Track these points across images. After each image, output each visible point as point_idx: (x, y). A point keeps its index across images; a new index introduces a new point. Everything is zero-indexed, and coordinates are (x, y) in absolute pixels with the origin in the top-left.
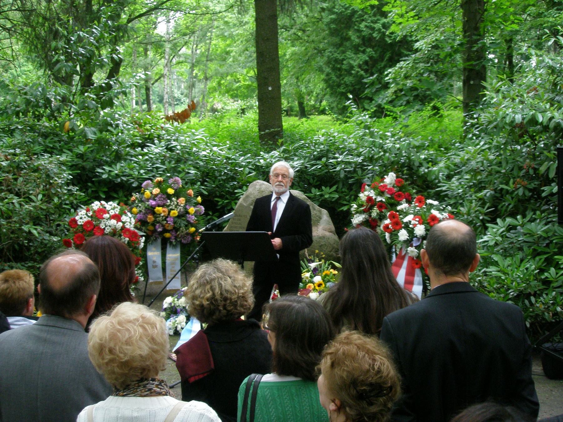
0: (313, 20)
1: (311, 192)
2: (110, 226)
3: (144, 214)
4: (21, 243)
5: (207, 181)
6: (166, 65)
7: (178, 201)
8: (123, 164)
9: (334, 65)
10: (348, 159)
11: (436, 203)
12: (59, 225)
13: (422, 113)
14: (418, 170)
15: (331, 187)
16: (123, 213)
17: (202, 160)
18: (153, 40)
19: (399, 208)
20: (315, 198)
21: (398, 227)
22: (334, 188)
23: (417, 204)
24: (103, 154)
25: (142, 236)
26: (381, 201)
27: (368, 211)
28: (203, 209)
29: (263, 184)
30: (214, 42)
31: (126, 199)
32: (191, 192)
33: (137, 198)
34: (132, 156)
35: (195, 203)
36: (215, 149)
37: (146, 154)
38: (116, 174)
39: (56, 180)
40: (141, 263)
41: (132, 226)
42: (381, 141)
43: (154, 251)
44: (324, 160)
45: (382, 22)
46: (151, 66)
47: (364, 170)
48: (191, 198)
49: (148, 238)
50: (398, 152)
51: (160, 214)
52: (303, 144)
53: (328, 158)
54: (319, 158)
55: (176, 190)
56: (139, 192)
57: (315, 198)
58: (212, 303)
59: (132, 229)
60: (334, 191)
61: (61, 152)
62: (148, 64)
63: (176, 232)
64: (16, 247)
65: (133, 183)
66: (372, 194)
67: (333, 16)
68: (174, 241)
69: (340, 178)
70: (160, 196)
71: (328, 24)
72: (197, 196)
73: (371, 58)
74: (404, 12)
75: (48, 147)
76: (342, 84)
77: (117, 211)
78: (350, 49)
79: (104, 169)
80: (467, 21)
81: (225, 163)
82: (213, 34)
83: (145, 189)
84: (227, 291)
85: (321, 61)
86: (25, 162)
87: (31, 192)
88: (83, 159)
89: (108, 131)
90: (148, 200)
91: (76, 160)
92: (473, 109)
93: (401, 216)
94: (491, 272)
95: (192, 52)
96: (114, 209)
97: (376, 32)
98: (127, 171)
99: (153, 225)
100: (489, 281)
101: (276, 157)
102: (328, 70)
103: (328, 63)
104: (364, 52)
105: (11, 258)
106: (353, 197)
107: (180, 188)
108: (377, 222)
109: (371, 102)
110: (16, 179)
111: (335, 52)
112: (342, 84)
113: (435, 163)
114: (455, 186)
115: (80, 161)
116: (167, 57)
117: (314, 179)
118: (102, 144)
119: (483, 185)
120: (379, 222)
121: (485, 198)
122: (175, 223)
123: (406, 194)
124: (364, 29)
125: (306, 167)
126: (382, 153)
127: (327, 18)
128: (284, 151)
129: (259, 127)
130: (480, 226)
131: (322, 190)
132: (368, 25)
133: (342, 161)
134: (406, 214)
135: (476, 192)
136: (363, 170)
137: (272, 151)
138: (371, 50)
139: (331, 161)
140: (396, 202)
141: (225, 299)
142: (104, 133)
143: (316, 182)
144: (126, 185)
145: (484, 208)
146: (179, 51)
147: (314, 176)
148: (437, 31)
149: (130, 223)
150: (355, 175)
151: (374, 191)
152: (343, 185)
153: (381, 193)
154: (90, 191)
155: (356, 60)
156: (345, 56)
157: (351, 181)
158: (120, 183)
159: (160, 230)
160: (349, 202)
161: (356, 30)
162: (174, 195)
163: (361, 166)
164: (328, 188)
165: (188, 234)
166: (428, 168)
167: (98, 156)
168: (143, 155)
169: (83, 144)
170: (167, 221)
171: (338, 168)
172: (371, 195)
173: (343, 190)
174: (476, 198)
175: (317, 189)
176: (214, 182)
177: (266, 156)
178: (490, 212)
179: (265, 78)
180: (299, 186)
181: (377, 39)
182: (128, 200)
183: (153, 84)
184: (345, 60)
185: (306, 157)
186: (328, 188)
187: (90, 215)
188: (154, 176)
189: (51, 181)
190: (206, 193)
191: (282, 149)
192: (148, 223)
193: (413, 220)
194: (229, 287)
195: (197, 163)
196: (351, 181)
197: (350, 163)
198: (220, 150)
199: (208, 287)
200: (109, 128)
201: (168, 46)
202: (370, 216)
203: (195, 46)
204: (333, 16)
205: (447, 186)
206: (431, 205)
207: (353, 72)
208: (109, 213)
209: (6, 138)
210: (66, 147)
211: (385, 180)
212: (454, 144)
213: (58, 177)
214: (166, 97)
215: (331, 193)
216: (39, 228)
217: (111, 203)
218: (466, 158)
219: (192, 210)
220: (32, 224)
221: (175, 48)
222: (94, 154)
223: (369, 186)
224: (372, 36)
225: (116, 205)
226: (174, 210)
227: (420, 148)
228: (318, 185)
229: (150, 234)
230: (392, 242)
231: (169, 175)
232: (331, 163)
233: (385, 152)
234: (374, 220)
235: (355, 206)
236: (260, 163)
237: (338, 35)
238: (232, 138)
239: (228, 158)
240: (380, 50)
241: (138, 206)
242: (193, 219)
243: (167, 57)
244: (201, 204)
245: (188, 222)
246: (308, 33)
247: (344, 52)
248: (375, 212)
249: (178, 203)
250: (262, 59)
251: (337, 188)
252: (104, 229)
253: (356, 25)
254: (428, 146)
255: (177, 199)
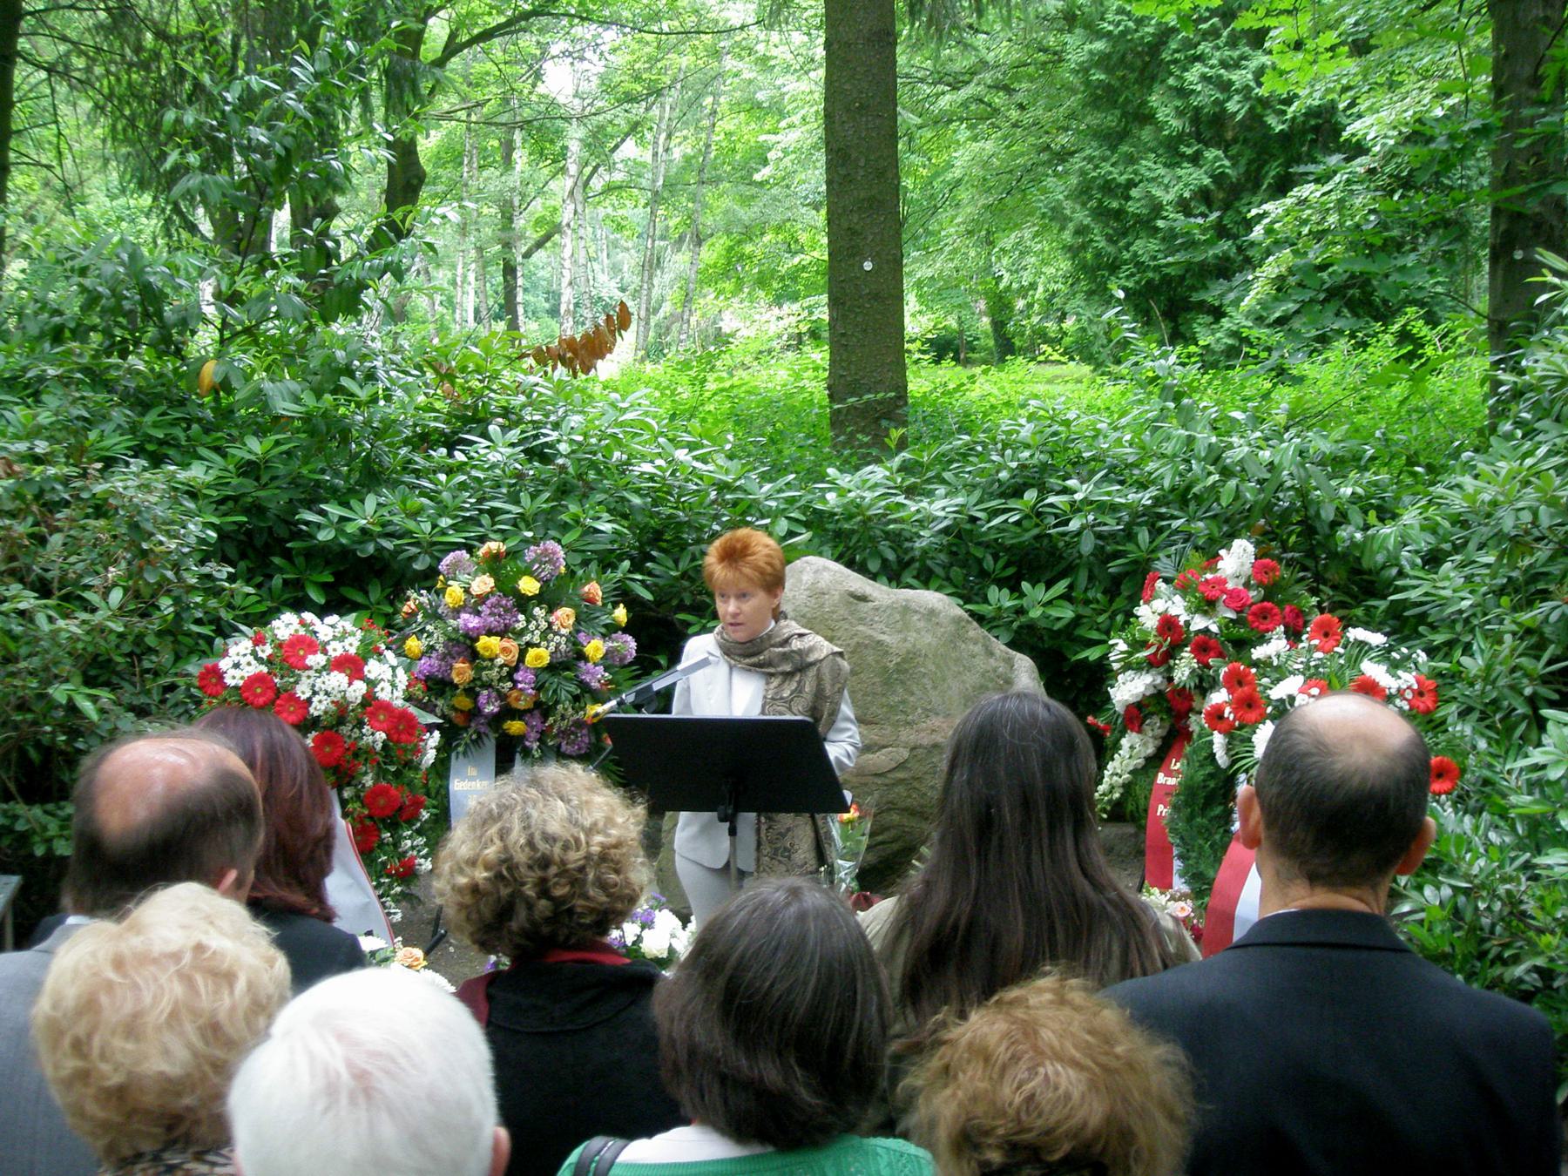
0: (1042, 57)
1: (986, 601)
2: (327, 694)
3: (443, 657)
4: (45, 740)
5: (653, 559)
6: (572, 193)
7: (552, 619)
8: (387, 495)
9: (1100, 202)
10: (1108, 494)
11: (1377, 639)
12: (172, 688)
13: (1365, 355)
14: (1331, 535)
15: (1049, 585)
16: (370, 650)
17: (637, 491)
18: (527, 113)
19: (1258, 653)
20: (1001, 618)
21: (1252, 716)
22: (1061, 587)
23: (1316, 642)
24: (322, 465)
25: (430, 728)
26: (1206, 630)
27: (1162, 662)
28: (633, 644)
29: (826, 569)
30: (726, 125)
31: (390, 610)
32: (594, 589)
33: (420, 606)
34: (417, 473)
35: (605, 626)
36: (681, 455)
37: (461, 468)
38: (363, 530)
39: (161, 543)
40: (425, 815)
41: (399, 693)
42: (1214, 439)
43: (472, 779)
44: (1031, 495)
45: (1253, 64)
46: (523, 195)
47: (1161, 530)
48: (597, 609)
49: (451, 733)
50: (1268, 476)
51: (492, 660)
52: (966, 445)
53: (1044, 490)
54: (1018, 493)
55: (545, 583)
56: (429, 590)
57: (1001, 618)
58: (499, 877)
59: (399, 703)
60: (1060, 597)
61: (189, 455)
62: (513, 190)
63: (545, 717)
64: (33, 754)
65: (413, 558)
66: (1178, 607)
67: (1099, 45)
68: (535, 745)
69: (1080, 556)
70: (493, 600)
71: (1083, 70)
72: (615, 605)
73: (1219, 178)
74: (1304, 31)
75: (150, 439)
76: (1125, 262)
77: (352, 646)
78: (1153, 150)
79: (323, 513)
80: (1506, 56)
81: (713, 502)
82: (722, 100)
83: (447, 579)
84: (550, 839)
85: (1057, 188)
86: (66, 481)
87: (87, 580)
88: (257, 479)
89: (338, 390)
90: (457, 612)
91: (235, 481)
92: (1521, 341)
93: (1265, 681)
94: (1549, 867)
95: (655, 154)
96: (341, 639)
97: (1236, 98)
98: (396, 519)
99: (471, 692)
100: (1541, 898)
101: (876, 485)
102: (1082, 216)
103: (1083, 193)
104: (1195, 160)
105: (12, 786)
106: (1119, 618)
107: (560, 577)
108: (1190, 698)
109: (1217, 321)
110: (42, 541)
111: (1105, 159)
112: (1125, 262)
113: (1386, 513)
114: (1450, 587)
115: (249, 485)
116: (573, 169)
117: (996, 558)
118: (324, 433)
119: (1541, 586)
120: (1197, 698)
121: (1547, 630)
122: (539, 688)
123: (1287, 609)
124: (1199, 88)
125: (973, 520)
126: (1216, 477)
127: (1079, 48)
128: (905, 468)
129: (829, 388)
130: (1524, 717)
131: (1022, 595)
132: (1211, 72)
133: (1086, 501)
134: (1279, 673)
135: (1515, 609)
136: (1155, 531)
137: (869, 464)
138: (1220, 153)
139: (1051, 499)
140: (1253, 636)
141: (544, 862)
142: (328, 397)
143: (1005, 567)
144: (395, 566)
145: (1538, 658)
146: (613, 150)
147: (996, 548)
148: (1422, 89)
149: (394, 686)
150: (1130, 547)
151: (1184, 598)
152: (1091, 578)
153: (1207, 606)
154: (277, 581)
155: (1169, 185)
156: (1135, 172)
157: (1114, 567)
158: (372, 556)
159: (491, 709)
160: (1107, 633)
161: (1170, 88)
162: (540, 599)
163: (1152, 519)
164: (1041, 587)
165: (579, 724)
166: (1366, 527)
167: (305, 471)
168: (450, 471)
169: (261, 432)
170: (515, 682)
171: (1074, 525)
172: (1173, 612)
173: (1090, 595)
174: (1514, 628)
175: (1006, 591)
176: (676, 562)
177: (845, 480)
178: (1551, 673)
179: (852, 232)
180: (948, 579)
181: (1239, 117)
182: (397, 612)
183: (527, 255)
184: (1136, 185)
185: (974, 486)
186: (1041, 587)
187: (264, 656)
188: (483, 539)
189: (145, 546)
190: (648, 596)
191: (897, 460)
192: (456, 687)
193: (1301, 691)
194: (554, 827)
195: (623, 499)
196: (1114, 567)
197: (1114, 508)
198: (696, 458)
199: (493, 830)
200: (345, 381)
201: (574, 138)
202: (1170, 679)
203: (663, 136)
204: (1099, 45)
205: (1426, 587)
206: (1361, 644)
207: (1160, 223)
208: (325, 652)
209: (16, 409)
210: (208, 439)
211: (1220, 564)
212: (1456, 455)
213: (168, 533)
214: (567, 296)
215: (1050, 603)
216: (105, 695)
217: (333, 619)
218: (1487, 497)
219: (595, 647)
220: (78, 679)
221: (599, 145)
222: (295, 464)
223: (1167, 581)
224: (1224, 110)
225: (349, 627)
226: (538, 645)
227: (1338, 465)
228: (1008, 578)
229: (458, 720)
230: (1234, 763)
231: (529, 534)
232: (1051, 505)
233: (1226, 473)
234: (1182, 692)
235: (1122, 646)
236: (825, 501)
237: (1114, 104)
238: (740, 419)
239: (723, 487)
240: (1249, 154)
241: (423, 631)
242: (596, 676)
243: (573, 169)
244: (625, 630)
245: (584, 686)
246: (1019, 97)
247: (1131, 160)
248: (1185, 667)
249: (550, 624)
250: (843, 172)
251: (1071, 587)
252: (309, 701)
253: (1172, 74)
254: (1373, 459)
255: (550, 611)
